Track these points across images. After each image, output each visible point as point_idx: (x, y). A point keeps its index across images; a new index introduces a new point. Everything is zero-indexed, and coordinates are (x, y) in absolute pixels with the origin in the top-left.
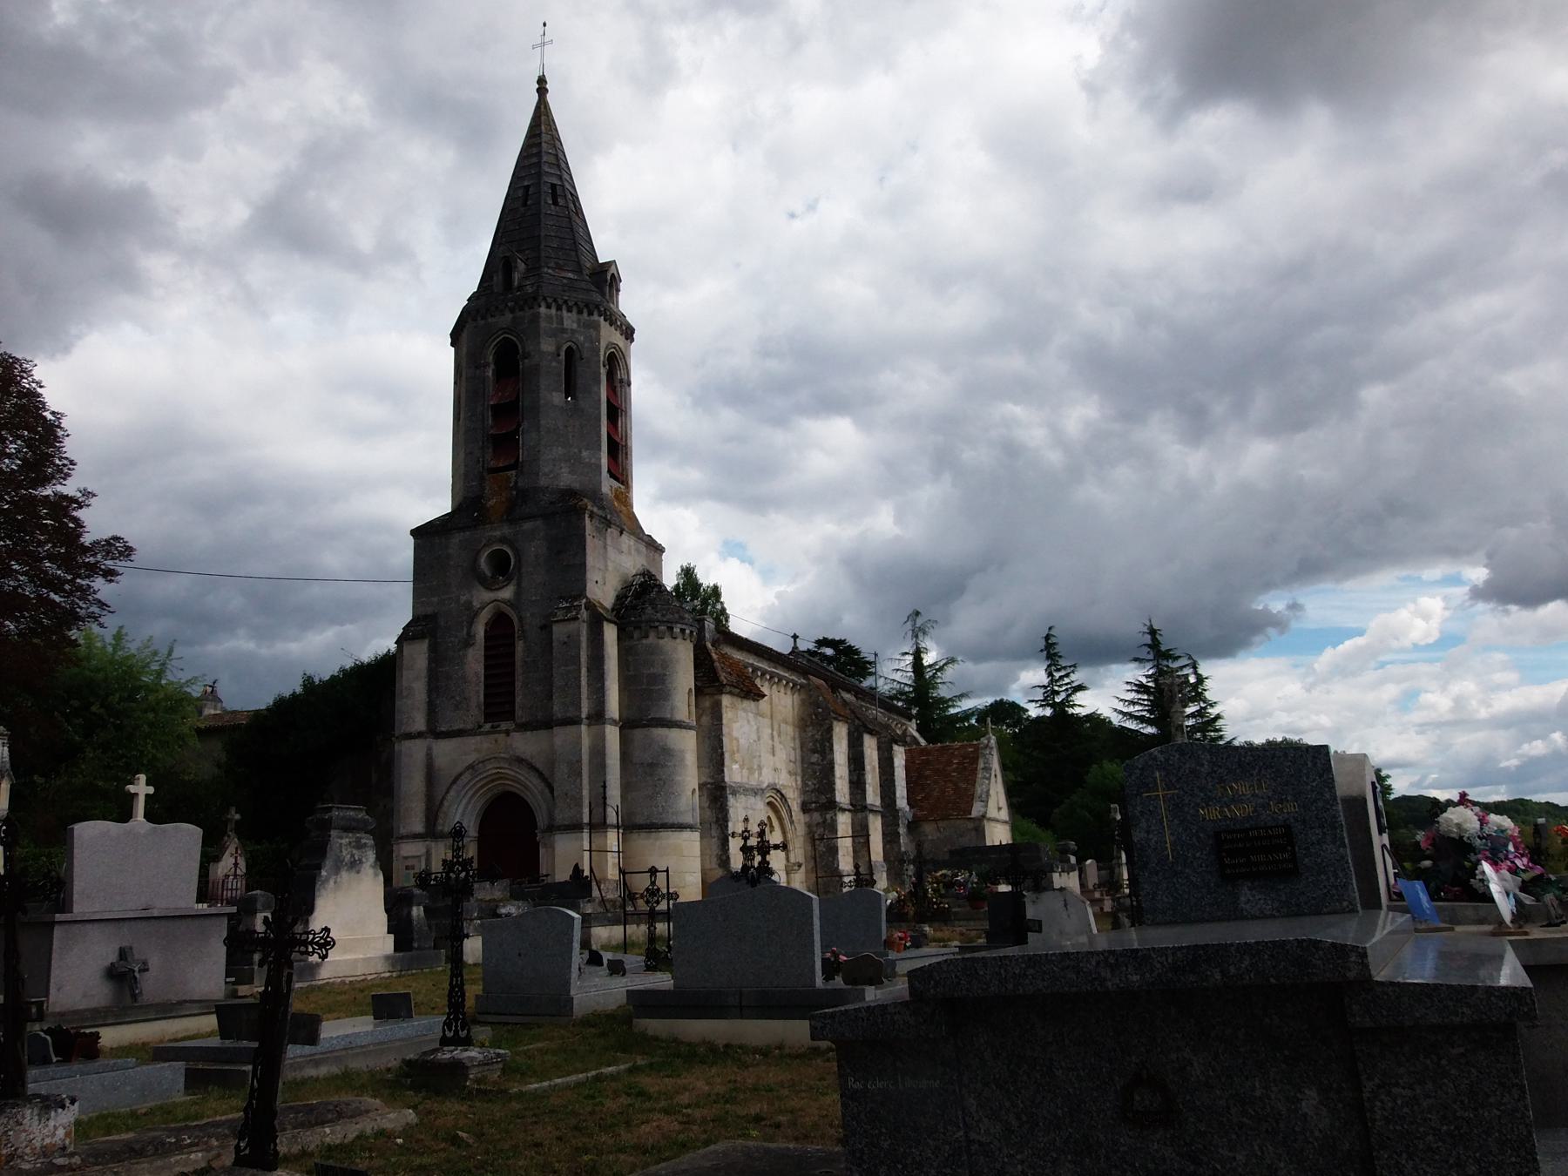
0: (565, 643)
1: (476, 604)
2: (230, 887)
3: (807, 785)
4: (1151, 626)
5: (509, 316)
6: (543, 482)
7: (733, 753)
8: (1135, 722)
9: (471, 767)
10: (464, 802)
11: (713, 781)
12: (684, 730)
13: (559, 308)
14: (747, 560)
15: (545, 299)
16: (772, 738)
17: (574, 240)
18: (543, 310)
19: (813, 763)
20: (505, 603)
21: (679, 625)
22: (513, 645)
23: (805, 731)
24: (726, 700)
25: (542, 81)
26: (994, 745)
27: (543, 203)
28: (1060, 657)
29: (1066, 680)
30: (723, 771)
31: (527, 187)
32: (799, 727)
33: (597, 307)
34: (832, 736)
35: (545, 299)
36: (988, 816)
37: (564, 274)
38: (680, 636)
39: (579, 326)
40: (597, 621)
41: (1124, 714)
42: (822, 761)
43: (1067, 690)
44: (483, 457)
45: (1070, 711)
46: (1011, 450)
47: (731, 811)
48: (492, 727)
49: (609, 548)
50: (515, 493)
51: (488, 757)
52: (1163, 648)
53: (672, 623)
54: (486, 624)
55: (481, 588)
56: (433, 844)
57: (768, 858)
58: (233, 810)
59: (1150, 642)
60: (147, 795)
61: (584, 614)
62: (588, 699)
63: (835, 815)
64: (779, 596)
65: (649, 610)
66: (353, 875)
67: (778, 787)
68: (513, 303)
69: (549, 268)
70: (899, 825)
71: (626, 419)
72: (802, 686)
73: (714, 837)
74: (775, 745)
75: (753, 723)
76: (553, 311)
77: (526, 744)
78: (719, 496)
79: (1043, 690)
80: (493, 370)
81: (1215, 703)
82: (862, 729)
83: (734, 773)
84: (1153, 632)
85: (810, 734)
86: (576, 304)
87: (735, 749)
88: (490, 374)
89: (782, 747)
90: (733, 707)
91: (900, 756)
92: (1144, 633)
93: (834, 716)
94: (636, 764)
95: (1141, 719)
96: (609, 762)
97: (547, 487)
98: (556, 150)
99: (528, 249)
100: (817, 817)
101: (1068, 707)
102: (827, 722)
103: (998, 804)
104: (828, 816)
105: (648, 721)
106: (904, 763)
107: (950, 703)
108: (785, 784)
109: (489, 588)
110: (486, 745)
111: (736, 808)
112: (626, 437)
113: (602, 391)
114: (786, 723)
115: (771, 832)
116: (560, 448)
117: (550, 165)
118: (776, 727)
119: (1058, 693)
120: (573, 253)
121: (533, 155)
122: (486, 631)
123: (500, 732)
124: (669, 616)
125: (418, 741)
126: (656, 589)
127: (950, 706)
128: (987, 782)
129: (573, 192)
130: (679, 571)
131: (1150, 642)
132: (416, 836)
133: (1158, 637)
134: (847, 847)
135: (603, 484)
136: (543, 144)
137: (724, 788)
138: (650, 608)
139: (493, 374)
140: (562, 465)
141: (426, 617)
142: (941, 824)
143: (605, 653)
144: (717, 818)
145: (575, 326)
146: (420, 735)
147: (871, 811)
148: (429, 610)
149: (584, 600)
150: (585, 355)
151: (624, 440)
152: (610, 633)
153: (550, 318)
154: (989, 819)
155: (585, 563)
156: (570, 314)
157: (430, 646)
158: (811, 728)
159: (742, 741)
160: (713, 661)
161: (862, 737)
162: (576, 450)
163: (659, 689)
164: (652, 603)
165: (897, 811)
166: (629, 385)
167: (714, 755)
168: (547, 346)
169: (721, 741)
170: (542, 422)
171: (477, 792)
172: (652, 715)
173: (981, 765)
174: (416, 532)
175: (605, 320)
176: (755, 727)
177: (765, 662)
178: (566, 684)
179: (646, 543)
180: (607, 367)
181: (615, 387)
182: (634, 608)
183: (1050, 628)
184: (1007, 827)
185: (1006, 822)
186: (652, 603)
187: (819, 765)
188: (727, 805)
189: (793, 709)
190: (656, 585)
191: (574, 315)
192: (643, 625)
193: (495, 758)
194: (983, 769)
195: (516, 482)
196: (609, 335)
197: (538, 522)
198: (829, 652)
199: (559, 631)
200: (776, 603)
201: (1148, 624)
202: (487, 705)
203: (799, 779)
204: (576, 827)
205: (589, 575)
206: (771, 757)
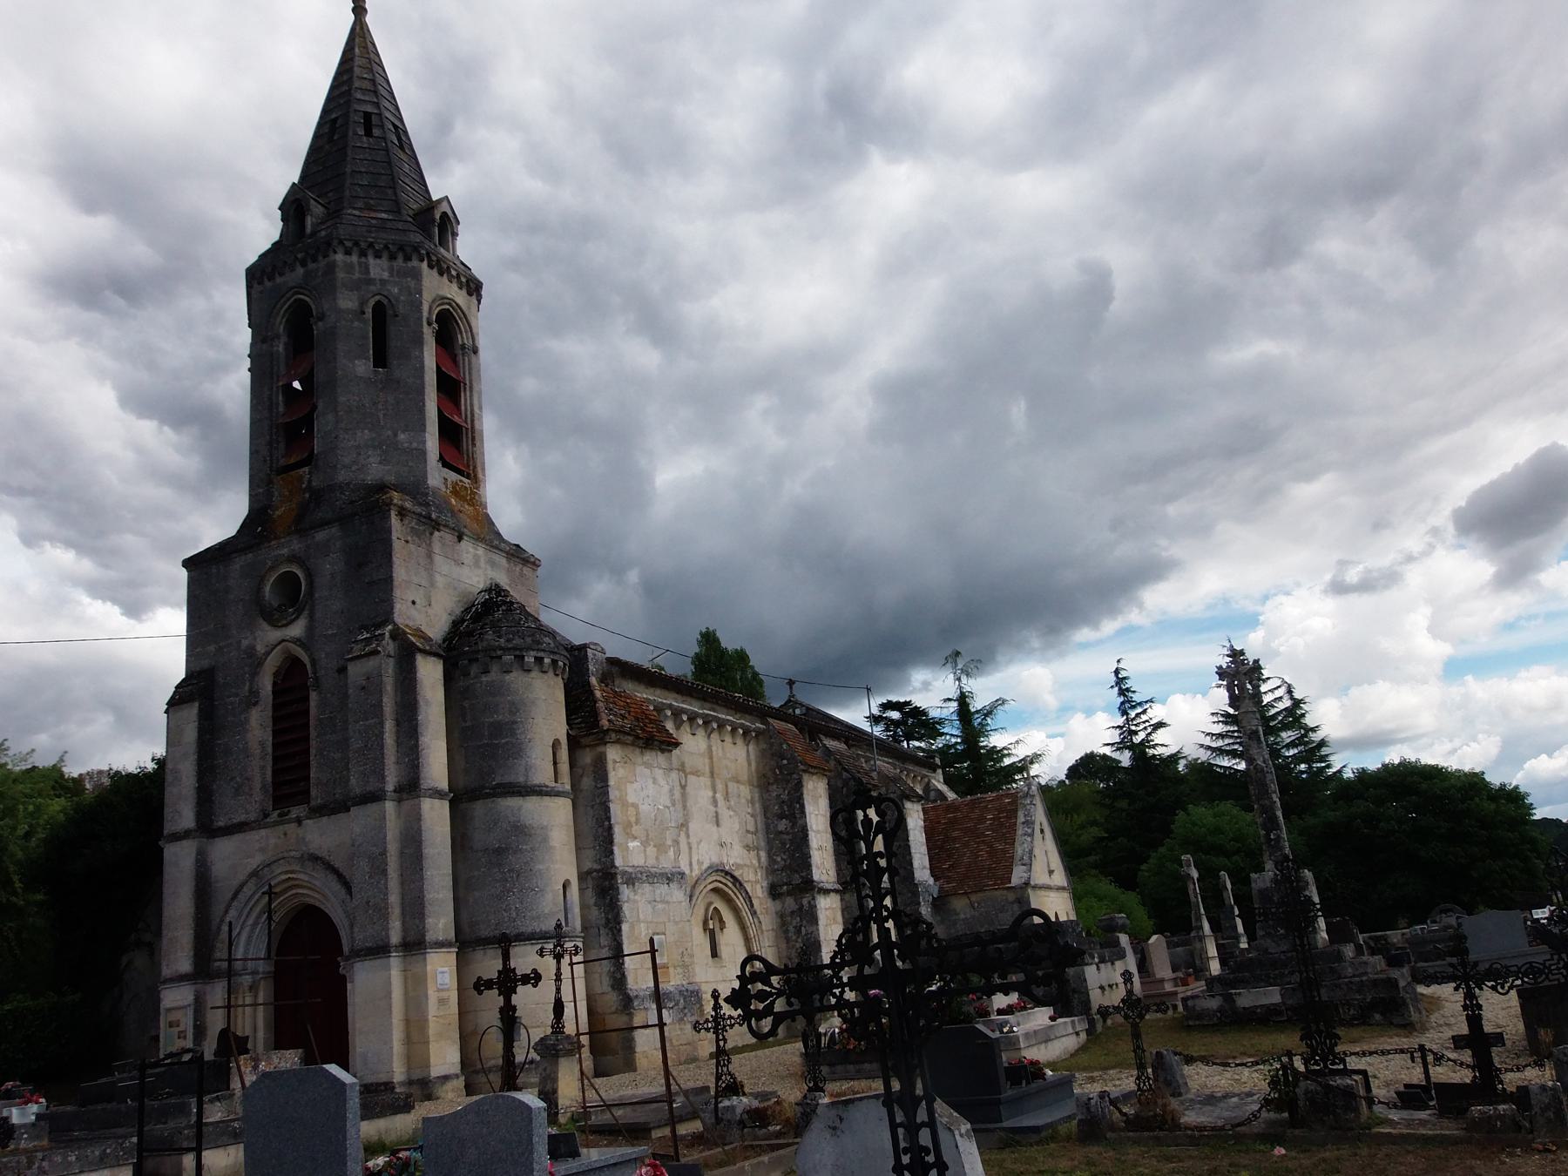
0: (363, 688)
1: (260, 649)
3: (775, 862)
5: (300, 271)
6: (342, 476)
8: (1226, 758)
9: (255, 874)
11: (599, 867)
13: (363, 254)
15: (341, 242)
16: (715, 802)
17: (392, 175)
18: (339, 257)
19: (781, 832)
20: (295, 643)
21: (532, 653)
22: (307, 699)
23: (768, 791)
24: (613, 753)
26: (1036, 793)
27: (351, 133)
28: (1134, 692)
29: (1144, 718)
30: (612, 852)
31: (335, 120)
32: (759, 786)
33: (416, 249)
34: (802, 794)
36: (1032, 883)
37: (373, 215)
39: (391, 275)
40: (407, 652)
41: (1213, 749)
42: (792, 827)
43: (1145, 728)
44: (271, 456)
45: (1151, 752)
47: (626, 908)
48: (280, 815)
49: (438, 559)
50: (307, 495)
51: (275, 858)
53: (521, 650)
54: (276, 675)
55: (265, 625)
57: (515, 999)
61: (389, 646)
63: (814, 899)
65: (490, 635)
67: (727, 868)
68: (303, 254)
69: (355, 209)
70: (919, 903)
71: (471, 396)
72: (759, 733)
73: (605, 946)
74: (720, 811)
75: (663, 782)
76: (354, 258)
77: (322, 835)
79: (1118, 731)
80: (285, 344)
81: (1317, 727)
83: (630, 853)
86: (386, 247)
87: (633, 819)
88: (281, 348)
89: (732, 813)
90: (626, 761)
91: (915, 815)
93: (802, 767)
94: (477, 851)
95: (1233, 754)
96: (428, 851)
97: (348, 484)
98: (374, 75)
99: (331, 191)
100: (790, 903)
101: (1149, 747)
102: (795, 776)
103: (1049, 866)
104: (805, 902)
105: (494, 788)
107: (1006, 752)
108: (739, 861)
109: (275, 624)
110: (273, 841)
111: (636, 902)
114: (738, 782)
115: (722, 929)
116: (366, 431)
118: (720, 786)
119: (1136, 733)
120: (390, 192)
121: (343, 83)
122: (275, 684)
123: (289, 821)
124: (517, 641)
125: (185, 843)
127: (1005, 756)
128: (1029, 839)
132: (182, 978)
135: (429, 476)
136: (356, 69)
137: (613, 876)
138: (490, 632)
139: (286, 349)
140: (370, 453)
141: (200, 673)
142: (974, 898)
143: (420, 698)
144: (607, 919)
145: (386, 275)
146: (186, 835)
148: (205, 663)
149: (390, 627)
150: (401, 309)
151: (469, 420)
152: (430, 673)
153: (349, 268)
154: (1035, 887)
155: (391, 577)
156: (378, 261)
157: (200, 710)
158: (775, 786)
159: (644, 808)
162: (390, 433)
163: (507, 743)
164: (495, 626)
165: (916, 886)
166: (475, 351)
167: (600, 830)
168: (347, 302)
169: (607, 809)
170: (342, 399)
172: (498, 780)
173: (1021, 818)
175: (431, 267)
176: (666, 788)
177: (694, 701)
178: (366, 746)
179: (507, 553)
180: (435, 325)
181: (456, 355)
184: (1066, 895)
185: (1063, 888)
186: (495, 626)
187: (788, 834)
188: (618, 900)
189: (750, 764)
190: (504, 603)
193: (284, 858)
194: (1023, 823)
195: (310, 481)
196: (434, 287)
197: (333, 530)
198: (895, 715)
199: (356, 671)
203: (763, 854)
204: (380, 950)
205: (397, 593)
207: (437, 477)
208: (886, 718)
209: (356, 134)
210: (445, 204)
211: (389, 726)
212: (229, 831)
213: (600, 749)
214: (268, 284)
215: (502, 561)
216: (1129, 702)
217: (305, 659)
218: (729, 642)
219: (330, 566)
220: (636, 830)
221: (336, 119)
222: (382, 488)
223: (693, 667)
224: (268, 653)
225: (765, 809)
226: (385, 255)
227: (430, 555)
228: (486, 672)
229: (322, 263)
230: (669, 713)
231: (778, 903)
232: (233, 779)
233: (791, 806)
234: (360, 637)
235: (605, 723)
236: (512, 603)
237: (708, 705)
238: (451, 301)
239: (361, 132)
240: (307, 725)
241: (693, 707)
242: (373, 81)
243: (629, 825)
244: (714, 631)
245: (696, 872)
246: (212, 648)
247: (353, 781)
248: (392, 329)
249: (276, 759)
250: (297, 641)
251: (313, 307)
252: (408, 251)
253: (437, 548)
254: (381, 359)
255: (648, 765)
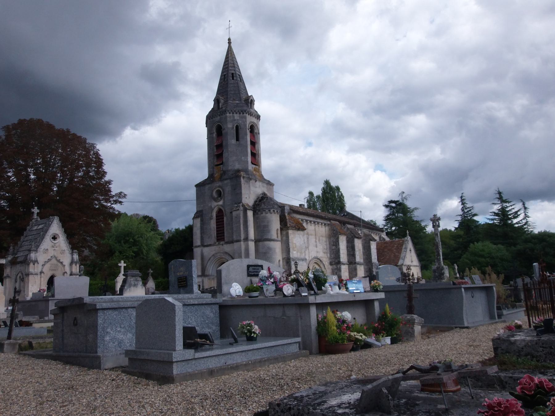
0: (236, 217)
1: (213, 206)
2: (546, 290)
4: (499, 191)
5: (219, 117)
6: (230, 168)
7: (294, 248)
9: (213, 255)
10: (212, 265)
12: (275, 242)
13: (233, 113)
14: (383, 170)
15: (228, 111)
16: (316, 242)
19: (333, 249)
21: (272, 209)
22: (223, 218)
24: (290, 232)
25: (229, 40)
28: (467, 204)
29: (470, 212)
30: (290, 254)
35: (228, 111)
36: (404, 264)
38: (273, 212)
40: (245, 210)
42: (336, 248)
46: (491, 120)
48: (218, 243)
50: (222, 172)
52: (504, 199)
53: (270, 209)
55: (214, 201)
56: (204, 278)
58: (150, 270)
59: (498, 197)
60: (124, 266)
61: (242, 208)
62: (244, 234)
64: (395, 183)
65: (263, 205)
66: (135, 288)
69: (231, 100)
72: (328, 225)
76: (231, 114)
78: (373, 148)
79: (460, 216)
82: (354, 237)
84: (500, 193)
85: (332, 240)
86: (238, 111)
87: (295, 247)
91: (374, 245)
92: (496, 193)
100: (335, 266)
104: (338, 266)
106: (375, 247)
112: (259, 150)
113: (248, 137)
114: (322, 237)
117: (232, 67)
118: (318, 238)
120: (238, 95)
121: (226, 68)
122: (216, 214)
123: (220, 245)
124: (269, 207)
126: (266, 198)
129: (239, 74)
130: (324, 182)
131: (498, 197)
133: (502, 195)
134: (346, 276)
136: (230, 61)
145: (238, 118)
146: (199, 246)
147: (358, 264)
148: (201, 209)
149: (241, 204)
152: (250, 214)
153: (230, 117)
156: (237, 115)
160: (286, 220)
161: (354, 240)
164: (264, 203)
168: (230, 125)
169: (289, 244)
170: (229, 149)
171: (216, 262)
173: (404, 247)
174: (197, 186)
175: (249, 115)
176: (303, 240)
180: (250, 129)
182: (258, 205)
183: (462, 194)
185: (417, 266)
186: (264, 203)
189: (326, 232)
190: (266, 197)
191: (238, 114)
192: (261, 210)
195: (223, 169)
196: (250, 120)
198: (394, 205)
199: (234, 213)
200: (395, 185)
201: (498, 190)
202: (217, 237)
205: (243, 196)
206: (316, 248)
207: (251, 167)
208: (390, 206)
209: (230, 79)
210: (251, 97)
211: (242, 226)
212: (207, 246)
213: (288, 231)
214: (212, 120)
215: (265, 185)
216: (465, 207)
217: (223, 210)
218: (333, 184)
219: (228, 189)
220: (295, 249)
221: (225, 75)
222: (239, 171)
223: (322, 192)
224: (215, 208)
225: (330, 243)
226: (238, 113)
227: (249, 187)
228: (262, 214)
229: (224, 116)
230: (305, 221)
231: (332, 266)
232: (208, 235)
233: (336, 243)
234: (235, 206)
235: (288, 225)
236: (267, 197)
237: (315, 218)
238: (253, 122)
239: (231, 79)
240: (223, 224)
241: (311, 219)
242: (234, 64)
243: (294, 248)
244: (329, 180)
245: (310, 258)
246: (202, 205)
247: (234, 237)
248: (240, 131)
249: (217, 231)
250: (221, 205)
251: (221, 124)
252: (243, 112)
253: (251, 185)
254: (237, 139)
255: (299, 234)
